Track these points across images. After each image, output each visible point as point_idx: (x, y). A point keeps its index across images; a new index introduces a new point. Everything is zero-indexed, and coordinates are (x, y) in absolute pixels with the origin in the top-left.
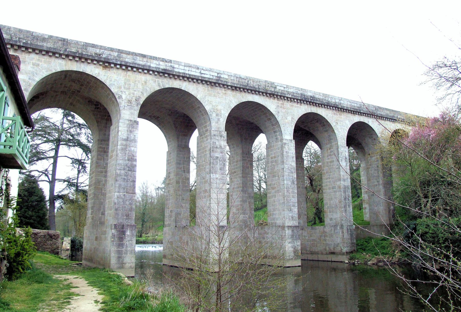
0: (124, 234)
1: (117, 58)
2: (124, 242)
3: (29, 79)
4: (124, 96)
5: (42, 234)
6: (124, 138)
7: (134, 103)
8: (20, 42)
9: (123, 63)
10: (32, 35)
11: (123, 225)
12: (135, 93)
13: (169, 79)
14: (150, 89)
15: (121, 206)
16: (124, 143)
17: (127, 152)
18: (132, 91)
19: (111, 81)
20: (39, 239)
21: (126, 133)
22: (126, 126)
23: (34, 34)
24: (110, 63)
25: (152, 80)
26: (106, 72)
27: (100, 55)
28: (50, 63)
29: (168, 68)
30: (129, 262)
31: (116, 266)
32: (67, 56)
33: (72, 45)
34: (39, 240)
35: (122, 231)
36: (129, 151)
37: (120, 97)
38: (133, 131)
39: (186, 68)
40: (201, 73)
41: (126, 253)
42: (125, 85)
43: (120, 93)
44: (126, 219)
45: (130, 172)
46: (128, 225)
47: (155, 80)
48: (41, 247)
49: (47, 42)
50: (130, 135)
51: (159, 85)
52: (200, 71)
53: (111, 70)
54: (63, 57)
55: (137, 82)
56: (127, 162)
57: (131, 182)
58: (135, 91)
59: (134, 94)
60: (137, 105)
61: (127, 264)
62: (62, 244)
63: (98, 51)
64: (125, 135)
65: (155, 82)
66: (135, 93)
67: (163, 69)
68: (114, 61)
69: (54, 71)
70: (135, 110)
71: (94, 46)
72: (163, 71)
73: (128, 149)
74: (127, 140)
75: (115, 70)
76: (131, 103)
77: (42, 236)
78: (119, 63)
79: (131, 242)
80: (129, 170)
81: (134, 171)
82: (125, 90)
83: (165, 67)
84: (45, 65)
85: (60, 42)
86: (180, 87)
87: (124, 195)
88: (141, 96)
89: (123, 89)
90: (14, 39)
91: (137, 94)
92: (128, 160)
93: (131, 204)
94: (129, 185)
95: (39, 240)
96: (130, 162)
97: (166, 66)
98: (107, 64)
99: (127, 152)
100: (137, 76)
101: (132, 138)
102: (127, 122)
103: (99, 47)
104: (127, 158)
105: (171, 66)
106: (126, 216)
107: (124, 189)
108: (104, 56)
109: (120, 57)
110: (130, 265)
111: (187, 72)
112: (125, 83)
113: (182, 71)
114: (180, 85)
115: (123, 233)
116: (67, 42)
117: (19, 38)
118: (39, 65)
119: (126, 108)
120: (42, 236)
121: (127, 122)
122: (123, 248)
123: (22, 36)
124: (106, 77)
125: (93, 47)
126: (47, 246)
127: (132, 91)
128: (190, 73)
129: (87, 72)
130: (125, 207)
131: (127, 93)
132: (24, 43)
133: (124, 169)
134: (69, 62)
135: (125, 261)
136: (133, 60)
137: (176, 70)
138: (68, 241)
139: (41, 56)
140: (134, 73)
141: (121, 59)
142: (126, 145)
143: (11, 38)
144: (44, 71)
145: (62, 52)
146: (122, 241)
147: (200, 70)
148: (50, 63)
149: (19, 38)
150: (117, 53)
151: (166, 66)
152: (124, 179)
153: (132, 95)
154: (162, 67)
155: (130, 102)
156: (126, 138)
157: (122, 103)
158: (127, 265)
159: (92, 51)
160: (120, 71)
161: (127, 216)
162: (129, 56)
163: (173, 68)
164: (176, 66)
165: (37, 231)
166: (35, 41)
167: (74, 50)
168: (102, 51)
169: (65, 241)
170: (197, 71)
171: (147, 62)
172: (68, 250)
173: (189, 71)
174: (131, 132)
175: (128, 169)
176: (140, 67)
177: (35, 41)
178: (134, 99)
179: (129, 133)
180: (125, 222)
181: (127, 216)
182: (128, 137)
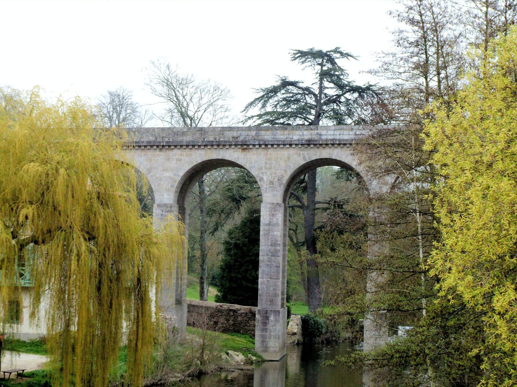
0: (268, 320)
1: (256, 137)
2: (268, 327)
3: (174, 175)
4: (265, 178)
5: (243, 312)
6: (266, 222)
7: (276, 183)
8: (163, 142)
9: (261, 143)
10: (173, 132)
11: (267, 311)
12: (278, 172)
13: (316, 150)
14: (294, 164)
15: (265, 292)
16: (267, 228)
17: (270, 237)
18: (273, 171)
19: (251, 163)
20: (240, 317)
21: (268, 217)
22: (267, 210)
23: (174, 130)
24: (248, 145)
25: (296, 154)
26: (245, 154)
27: (237, 138)
28: (191, 155)
29: (316, 137)
30: (272, 346)
31: (260, 350)
32: (206, 146)
33: (209, 133)
34: (239, 319)
35: (266, 316)
36: (272, 235)
37: (262, 179)
38: (276, 214)
39: (336, 132)
40: (356, 134)
41: (270, 338)
42: (266, 165)
43: (261, 175)
44: (270, 305)
45: (273, 258)
46: (271, 311)
47: (300, 154)
48: (242, 328)
49: (187, 136)
50: (273, 219)
51: (304, 158)
52: (355, 133)
53: (250, 150)
54: (202, 147)
55: (279, 160)
56: (270, 247)
57: (275, 267)
58: (277, 170)
59: (276, 173)
60: (280, 185)
61: (271, 349)
62: (288, 325)
63: (235, 134)
64: (267, 220)
65: (300, 155)
66: (278, 172)
67: (307, 141)
68: (252, 142)
69: (195, 163)
70: (277, 191)
71: (230, 129)
72: (308, 143)
73: (271, 233)
74: (269, 224)
75: (254, 151)
76: (273, 184)
77: (243, 314)
78: (257, 143)
79: (274, 327)
80: (272, 256)
81: (277, 256)
82: (266, 171)
83: (310, 137)
84: (187, 159)
85: (198, 133)
86: (331, 156)
87: (268, 281)
88: (284, 175)
89: (264, 170)
90: (159, 140)
91: (279, 173)
92: (271, 245)
93: (274, 290)
94: (273, 271)
95: (239, 319)
96: (273, 248)
97: (311, 135)
98: (245, 147)
99: (270, 237)
100: (279, 153)
101: (275, 222)
102: (269, 206)
103: (236, 130)
104: (269, 244)
105: (317, 134)
106: (270, 301)
107: (268, 274)
108: (241, 138)
109: (258, 136)
110: (274, 349)
111: (338, 137)
112: (266, 163)
113: (332, 137)
114: (330, 154)
115: (267, 318)
116: (205, 131)
117: (163, 137)
118: (181, 160)
119: (268, 190)
120: (243, 314)
121: (269, 206)
122: (266, 332)
123: (164, 135)
124: (246, 160)
125: (230, 131)
126: (250, 328)
127: (273, 171)
128: (341, 137)
129: (226, 159)
130: (269, 293)
131: (268, 174)
132: (167, 142)
133: (267, 255)
134: (209, 151)
135: (269, 346)
136: (273, 136)
137: (324, 137)
138: (296, 321)
139: (183, 150)
140: (275, 150)
141: (260, 138)
142: (269, 230)
143: (156, 138)
144: (186, 165)
145: (200, 144)
146: (266, 326)
147: (354, 131)
148: (191, 155)
149: (163, 137)
150: (255, 132)
151: (311, 135)
152: (268, 265)
153: (273, 175)
154: (306, 138)
155: (272, 183)
156: (268, 222)
157: (264, 185)
158: (271, 349)
159: (229, 136)
160: (260, 150)
161: (272, 301)
162: (268, 133)
163: (321, 135)
164: (324, 132)
165: (237, 307)
166: (176, 137)
167: (211, 139)
168: (239, 132)
169: (292, 320)
170: (351, 133)
171: (289, 135)
172: (294, 334)
173: (339, 135)
174: (273, 215)
175: (271, 254)
176: (280, 143)
177: (176, 137)
178: (276, 180)
179: (271, 217)
180: (269, 308)
181: (272, 301)
182: (270, 222)
